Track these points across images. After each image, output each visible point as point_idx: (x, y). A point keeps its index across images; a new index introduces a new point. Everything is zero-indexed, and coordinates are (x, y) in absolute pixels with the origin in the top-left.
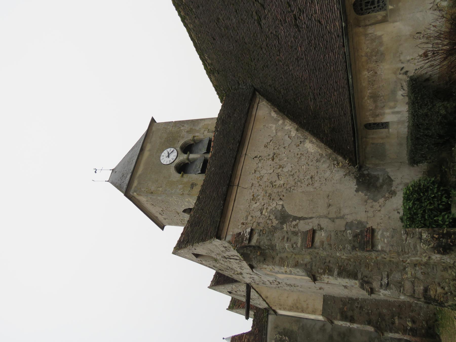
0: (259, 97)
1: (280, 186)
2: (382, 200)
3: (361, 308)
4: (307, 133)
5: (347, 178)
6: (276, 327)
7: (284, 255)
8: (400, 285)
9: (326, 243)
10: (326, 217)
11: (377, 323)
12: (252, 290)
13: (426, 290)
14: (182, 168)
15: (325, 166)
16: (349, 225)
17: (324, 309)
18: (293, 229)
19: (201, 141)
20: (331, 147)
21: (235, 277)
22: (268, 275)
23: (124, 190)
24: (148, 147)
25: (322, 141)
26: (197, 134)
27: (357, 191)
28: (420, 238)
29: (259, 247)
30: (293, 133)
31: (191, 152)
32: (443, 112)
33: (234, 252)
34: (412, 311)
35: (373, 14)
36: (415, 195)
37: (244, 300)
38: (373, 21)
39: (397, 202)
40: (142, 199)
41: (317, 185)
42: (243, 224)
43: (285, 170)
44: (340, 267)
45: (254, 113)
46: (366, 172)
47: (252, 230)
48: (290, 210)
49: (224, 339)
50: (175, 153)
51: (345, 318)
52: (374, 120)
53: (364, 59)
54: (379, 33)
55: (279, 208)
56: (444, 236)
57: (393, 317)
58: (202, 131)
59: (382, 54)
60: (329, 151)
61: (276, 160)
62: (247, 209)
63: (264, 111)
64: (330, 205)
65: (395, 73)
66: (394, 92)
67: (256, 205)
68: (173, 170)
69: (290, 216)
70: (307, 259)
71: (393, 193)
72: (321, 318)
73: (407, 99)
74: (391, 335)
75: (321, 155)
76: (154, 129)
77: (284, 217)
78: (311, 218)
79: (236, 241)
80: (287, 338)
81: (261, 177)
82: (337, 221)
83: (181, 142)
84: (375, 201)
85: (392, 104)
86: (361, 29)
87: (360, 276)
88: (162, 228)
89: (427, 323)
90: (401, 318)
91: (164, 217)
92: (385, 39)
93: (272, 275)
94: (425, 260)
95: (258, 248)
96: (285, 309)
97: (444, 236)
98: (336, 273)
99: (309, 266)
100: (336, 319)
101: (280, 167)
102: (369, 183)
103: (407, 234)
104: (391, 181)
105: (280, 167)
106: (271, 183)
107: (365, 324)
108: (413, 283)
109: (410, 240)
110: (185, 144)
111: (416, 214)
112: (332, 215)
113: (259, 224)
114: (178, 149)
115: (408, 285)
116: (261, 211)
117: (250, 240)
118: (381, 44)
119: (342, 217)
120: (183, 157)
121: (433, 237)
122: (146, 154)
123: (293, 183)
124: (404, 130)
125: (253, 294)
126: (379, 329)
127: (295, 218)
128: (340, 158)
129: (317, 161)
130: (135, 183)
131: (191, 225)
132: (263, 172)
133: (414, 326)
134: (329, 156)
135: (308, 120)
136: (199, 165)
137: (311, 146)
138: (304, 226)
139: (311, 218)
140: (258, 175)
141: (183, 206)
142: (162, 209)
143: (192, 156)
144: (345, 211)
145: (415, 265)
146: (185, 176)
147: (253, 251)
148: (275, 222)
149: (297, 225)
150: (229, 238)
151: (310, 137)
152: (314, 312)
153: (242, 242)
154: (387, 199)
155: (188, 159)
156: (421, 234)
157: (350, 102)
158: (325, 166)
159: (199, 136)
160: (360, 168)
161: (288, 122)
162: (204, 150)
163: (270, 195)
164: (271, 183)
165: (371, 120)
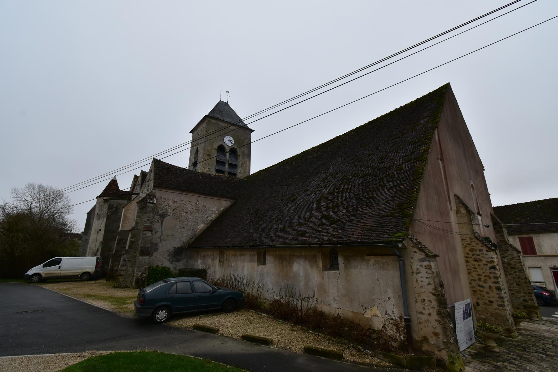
0: (233, 201)
4: (209, 225)
6: (120, 205)
7: (142, 217)
8: (124, 265)
10: (162, 235)
13: (122, 275)
14: (221, 149)
16: (156, 244)
17: (124, 231)
19: (237, 159)
27: (174, 248)
30: (210, 218)
40: (204, 125)
43: (189, 216)
44: (135, 241)
48: (167, 219)
51: (119, 240)
55: (168, 214)
60: (197, 235)
62: (170, 199)
63: (225, 204)
64: (168, 236)
68: (220, 143)
70: (139, 228)
71: (171, 262)
75: (196, 231)
76: (247, 131)
77: (163, 216)
82: (159, 240)
94: (135, 275)
106: (183, 210)
108: (125, 270)
112: (162, 237)
113: (161, 205)
115: (124, 268)
116: (168, 205)
119: (161, 241)
120: (228, 150)
124: (196, 267)
127: (162, 221)
128: (193, 240)
129: (193, 230)
130: (213, 121)
131: (168, 168)
134: (195, 235)
135: (214, 227)
136: (221, 159)
137: (201, 227)
138: (157, 226)
140: (188, 203)
143: (228, 154)
144: (164, 243)
148: (161, 212)
150: (154, 191)
152: (122, 226)
154: (169, 260)
158: (190, 233)
159: (240, 158)
161: (217, 215)
162: (230, 162)
164: (183, 210)
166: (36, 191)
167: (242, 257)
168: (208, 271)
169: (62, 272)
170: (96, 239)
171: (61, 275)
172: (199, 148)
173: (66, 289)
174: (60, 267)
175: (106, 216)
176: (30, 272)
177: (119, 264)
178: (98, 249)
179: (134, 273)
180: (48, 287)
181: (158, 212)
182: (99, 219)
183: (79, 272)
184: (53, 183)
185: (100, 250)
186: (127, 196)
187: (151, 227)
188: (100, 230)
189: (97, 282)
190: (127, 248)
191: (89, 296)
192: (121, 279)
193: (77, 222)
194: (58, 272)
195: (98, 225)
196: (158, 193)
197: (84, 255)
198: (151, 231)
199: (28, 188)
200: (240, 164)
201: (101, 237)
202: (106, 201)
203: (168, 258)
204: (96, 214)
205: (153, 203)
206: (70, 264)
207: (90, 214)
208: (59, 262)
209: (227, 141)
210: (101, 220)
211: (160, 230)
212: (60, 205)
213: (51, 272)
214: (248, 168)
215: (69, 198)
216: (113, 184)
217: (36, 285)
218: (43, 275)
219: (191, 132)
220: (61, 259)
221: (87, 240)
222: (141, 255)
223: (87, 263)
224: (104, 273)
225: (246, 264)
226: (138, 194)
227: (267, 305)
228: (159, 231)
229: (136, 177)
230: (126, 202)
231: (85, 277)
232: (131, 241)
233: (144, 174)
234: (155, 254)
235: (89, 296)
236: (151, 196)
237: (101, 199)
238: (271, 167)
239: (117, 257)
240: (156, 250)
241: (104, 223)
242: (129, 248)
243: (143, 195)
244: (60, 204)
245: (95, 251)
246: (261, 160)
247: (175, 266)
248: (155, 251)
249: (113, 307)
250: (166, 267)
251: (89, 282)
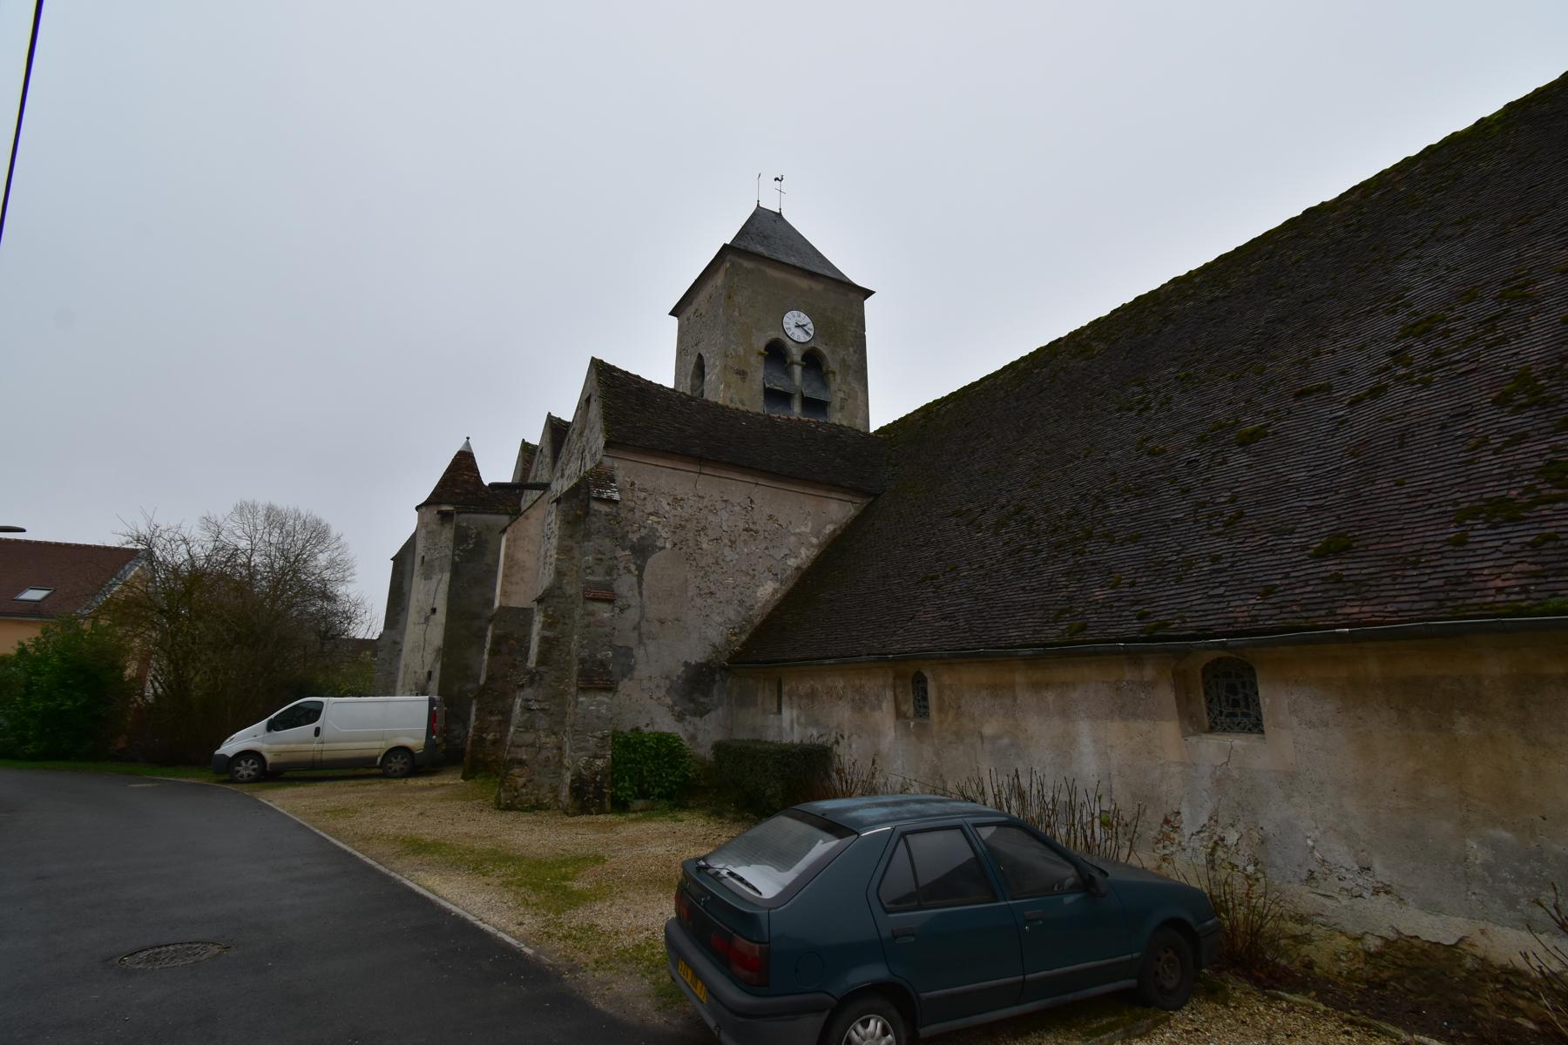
0: (861, 502)
1: (697, 543)
2: (669, 701)
3: (514, 666)
4: (790, 584)
5: (710, 649)
7: (576, 553)
8: (527, 727)
9: (592, 619)
10: (642, 617)
12: (539, 493)
13: (521, 763)
14: (776, 352)
15: (732, 614)
16: (627, 652)
17: (511, 609)
18: (621, 566)
20: (764, 623)
21: (559, 464)
23: (742, 244)
24: (818, 287)
25: (776, 608)
26: (838, 378)
27: (686, 664)
28: (596, 757)
29: (587, 514)
30: (792, 562)
31: (804, 368)
32: (769, 792)
33: (589, 465)
35: (911, 698)
36: (667, 750)
37: (530, 481)
38: (900, 697)
39: (666, 724)
40: (719, 279)
41: (699, 601)
42: (633, 484)
43: (727, 551)
44: (557, 639)
45: (833, 495)
46: (717, 677)
47: (616, 502)
48: (654, 562)
50: (803, 338)
51: (497, 641)
53: (857, 682)
54: (884, 705)
56: (599, 788)
58: (844, 387)
59: (861, 709)
60: (757, 621)
61: (745, 536)
62: (659, 490)
63: (837, 511)
64: (662, 622)
65: (838, 726)
66: (816, 723)
67: (664, 503)
68: (772, 334)
69: (645, 561)
70: (570, 590)
71: (680, 718)
72: (497, 604)
73: (807, 741)
74: (474, 709)
75: (751, 608)
76: (852, 296)
77: (643, 551)
78: (641, 594)
79: (599, 475)
81: (714, 512)
82: (635, 634)
83: (824, 350)
84: (668, 691)
85: (802, 720)
86: (891, 680)
87: (541, 669)
88: (673, 313)
92: (877, 715)
94: (566, 762)
95: (587, 512)
96: (508, 547)
97: (599, 788)
98: (547, 633)
99: (557, 592)
100: (495, 627)
101: (733, 542)
102: (698, 684)
103: (603, 738)
104: (701, 716)
105: (733, 542)
108: (532, 745)
109: (592, 741)
110: (822, 356)
111: (635, 751)
112: (645, 627)
113: (632, 510)
114: (812, 345)
115: (529, 737)
116: (655, 514)
117: (599, 500)
118: (873, 709)
119: (641, 642)
121: (597, 773)
122: (804, 283)
123: (703, 564)
124: (771, 736)
125: (536, 494)
126: (482, 691)
127: (641, 569)
128: (744, 637)
129: (741, 602)
130: (747, 264)
132: (724, 515)
134: (749, 620)
135: (808, 588)
136: (779, 385)
137: (767, 591)
138: (625, 585)
139: (641, 594)
143: (797, 370)
145: (560, 748)
146: (761, 358)
147: (580, 504)
148: (634, 537)
149: (629, 571)
150: (608, 462)
151: (785, 588)
152: (504, 593)
153: (597, 486)
154: (671, 708)
155: (793, 363)
156: (603, 757)
158: (732, 614)
159: (836, 382)
160: (723, 668)
161: (816, 552)
162: (807, 393)
163: (683, 527)
165: (785, 689)
166: (260, 521)
167: (1050, 696)
168: (839, 750)
169: (326, 746)
170: (424, 640)
171: (325, 756)
172: (706, 356)
173: (336, 812)
175: (448, 567)
176: (230, 747)
177: (506, 723)
178: (430, 673)
179: (561, 755)
180: (280, 799)
181: (624, 537)
182: (427, 577)
183: (377, 747)
184: (300, 497)
185: (436, 675)
186: (505, 498)
187: (608, 587)
188: (434, 611)
189: (436, 780)
190: (532, 662)
191: (417, 847)
192: (519, 776)
193: (365, 599)
194: (314, 746)
196: (624, 469)
197: (389, 690)
198: (610, 601)
199: (241, 515)
200: (836, 403)
201: (436, 635)
202: (445, 517)
203: (669, 701)
204: (418, 560)
205: (610, 501)
206: (357, 721)
207: (402, 562)
208: (313, 714)
209: (792, 325)
210: (435, 581)
211: (635, 602)
212: (322, 559)
214: (861, 414)
215: (343, 540)
216: (464, 463)
217: (246, 790)
218: (269, 758)
219: (674, 312)
221: (396, 643)
222: (583, 690)
223: (401, 717)
224: (457, 750)
225: (1084, 730)
226: (545, 487)
227: (1324, 952)
228: (633, 603)
229: (527, 449)
230: (505, 519)
231: (397, 764)
232: (544, 640)
233: (555, 428)
234: (625, 686)
235: (417, 847)
236: (601, 477)
237: (432, 512)
238: (973, 385)
239: (495, 696)
240: (628, 670)
241: (444, 587)
242: (540, 662)
243: (560, 486)
244: (320, 556)
246: (893, 392)
247: (691, 729)
248: (624, 676)
249: (532, 923)
250: (668, 736)
251: (411, 782)
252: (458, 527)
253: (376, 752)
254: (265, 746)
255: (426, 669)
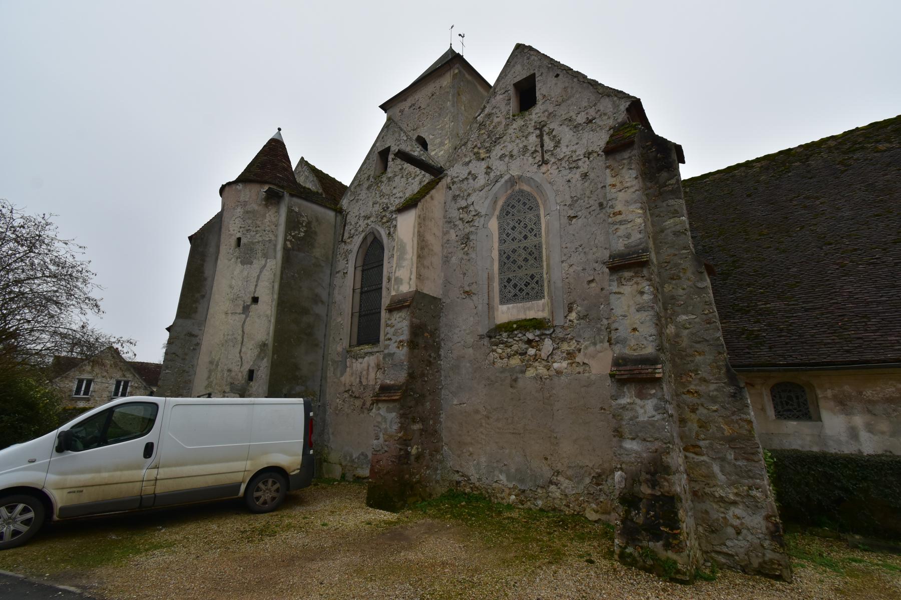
3: (430, 364)
11: (412, 389)
22: (495, 202)
34: (431, 455)
49: (279, 129)
52: (826, 398)
57: (423, 420)
80: (302, 234)
88: (384, 107)
89: (419, 482)
90: (421, 435)
91: (407, 109)
93: (494, 209)
107: (409, 368)
133: (412, 458)
141: (431, 137)
142: (423, 107)
157: (884, 361)
169: (163, 472)
171: (160, 489)
174: (149, 450)
178: (251, 374)
183: (238, 470)
188: (255, 300)
195: (247, 280)
207: (203, 243)
208: (145, 421)
210: (257, 264)
213: (105, 476)
218: (59, 499)
220: (155, 406)
221: (191, 335)
231: (267, 492)
245: (240, 376)
252: (290, 211)
253: (238, 477)
254: (52, 478)
255: (246, 368)
